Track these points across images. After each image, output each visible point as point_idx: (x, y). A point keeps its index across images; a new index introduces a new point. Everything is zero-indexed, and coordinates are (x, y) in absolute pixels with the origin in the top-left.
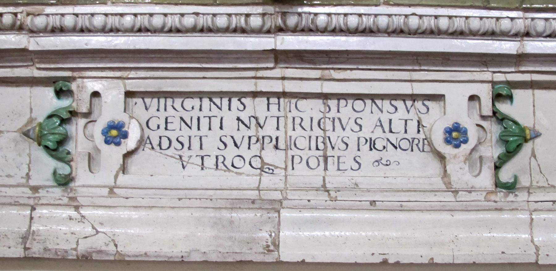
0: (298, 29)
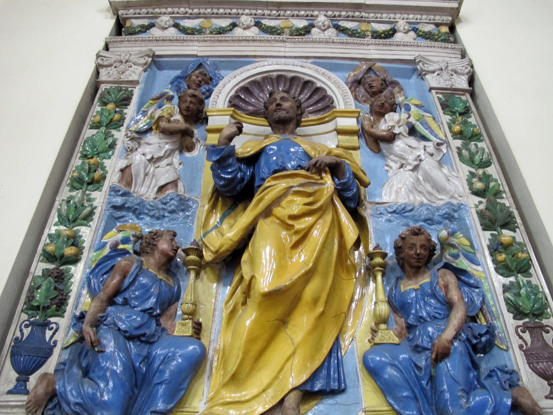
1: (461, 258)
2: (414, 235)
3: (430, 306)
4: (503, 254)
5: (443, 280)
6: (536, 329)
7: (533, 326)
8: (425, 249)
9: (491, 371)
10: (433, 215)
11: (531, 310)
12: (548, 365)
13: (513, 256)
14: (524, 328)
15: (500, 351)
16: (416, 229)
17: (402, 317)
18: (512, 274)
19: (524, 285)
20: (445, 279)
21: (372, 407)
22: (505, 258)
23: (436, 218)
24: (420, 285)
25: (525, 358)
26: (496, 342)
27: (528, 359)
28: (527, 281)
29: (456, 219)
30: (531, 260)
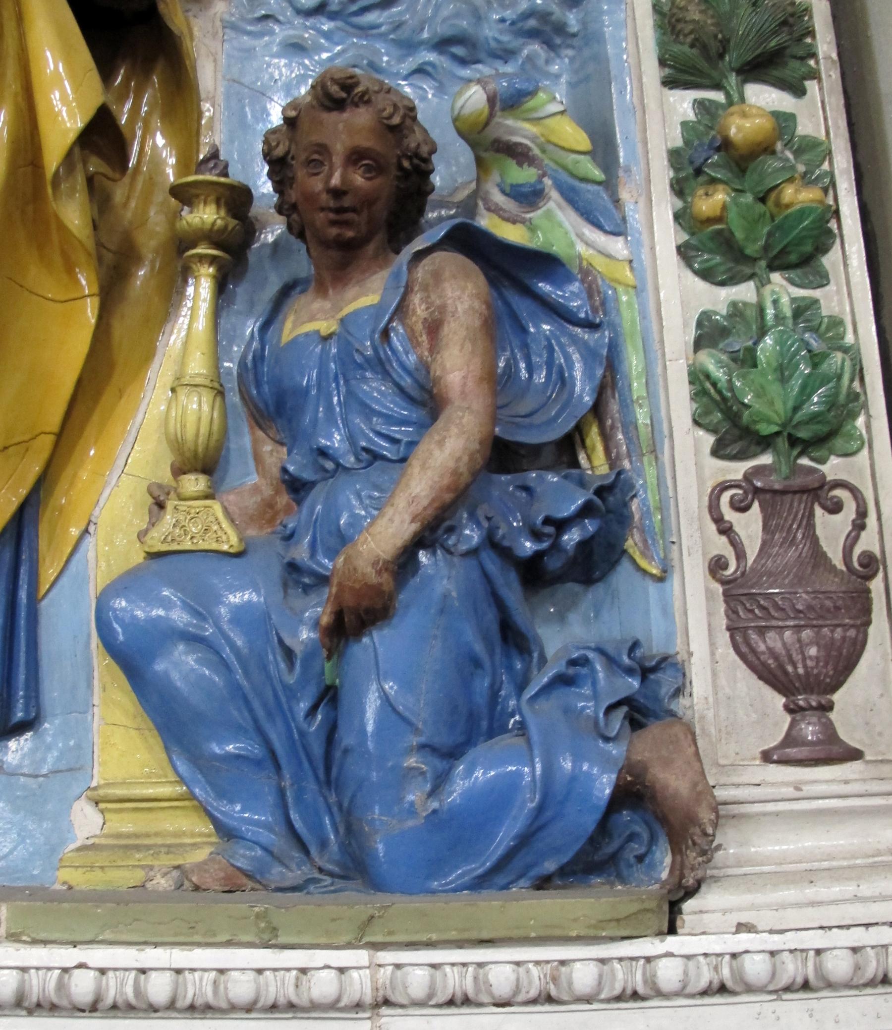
0: (342, 1004)
1: (551, 205)
2: (329, 109)
3: (368, 412)
4: (721, 187)
5: (426, 300)
6: (788, 498)
7: (777, 486)
8: (369, 169)
9: (573, 663)
10: (478, 17)
11: (784, 425)
12: (799, 641)
13: (763, 200)
14: (746, 492)
15: (638, 576)
16: (334, 81)
17: (282, 444)
18: (748, 271)
19: (779, 318)
20: (433, 297)
21: (123, 783)
22: (724, 207)
23: (490, 32)
24: (342, 321)
25: (722, 608)
26: (629, 544)
27: (731, 612)
28: (793, 300)
29: (574, 35)
30: (837, 213)
